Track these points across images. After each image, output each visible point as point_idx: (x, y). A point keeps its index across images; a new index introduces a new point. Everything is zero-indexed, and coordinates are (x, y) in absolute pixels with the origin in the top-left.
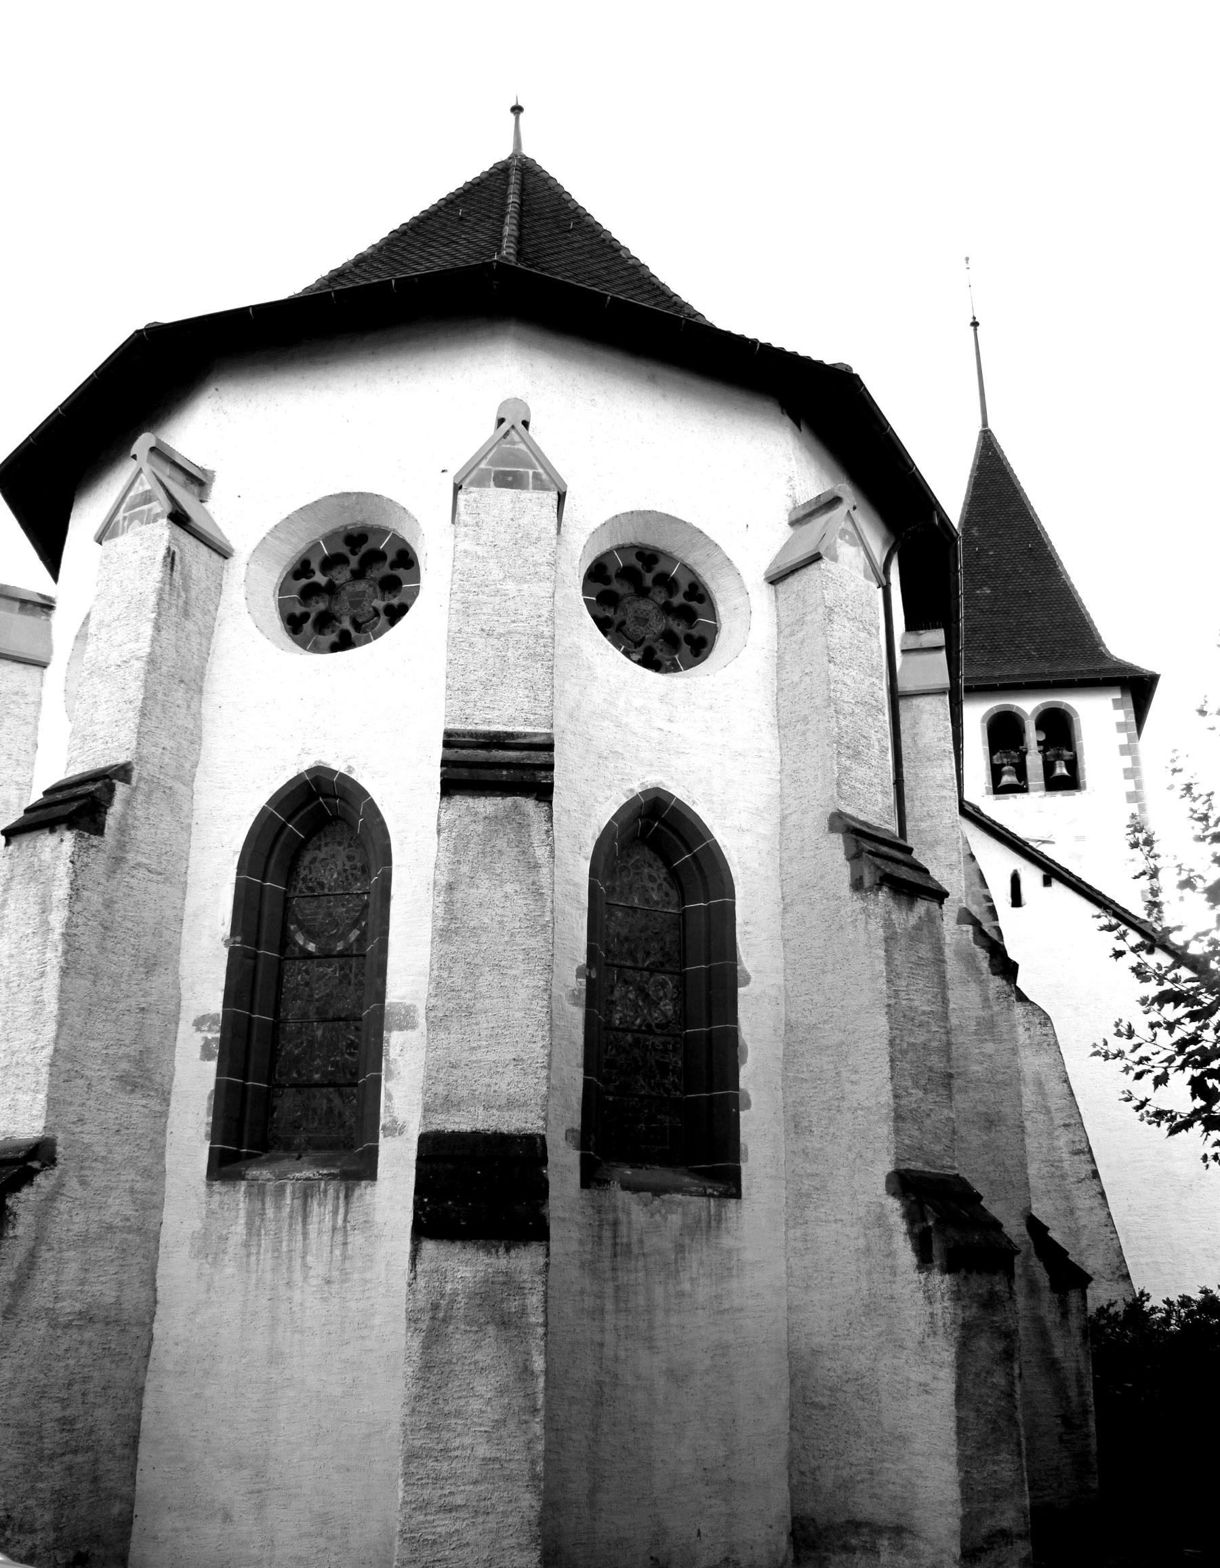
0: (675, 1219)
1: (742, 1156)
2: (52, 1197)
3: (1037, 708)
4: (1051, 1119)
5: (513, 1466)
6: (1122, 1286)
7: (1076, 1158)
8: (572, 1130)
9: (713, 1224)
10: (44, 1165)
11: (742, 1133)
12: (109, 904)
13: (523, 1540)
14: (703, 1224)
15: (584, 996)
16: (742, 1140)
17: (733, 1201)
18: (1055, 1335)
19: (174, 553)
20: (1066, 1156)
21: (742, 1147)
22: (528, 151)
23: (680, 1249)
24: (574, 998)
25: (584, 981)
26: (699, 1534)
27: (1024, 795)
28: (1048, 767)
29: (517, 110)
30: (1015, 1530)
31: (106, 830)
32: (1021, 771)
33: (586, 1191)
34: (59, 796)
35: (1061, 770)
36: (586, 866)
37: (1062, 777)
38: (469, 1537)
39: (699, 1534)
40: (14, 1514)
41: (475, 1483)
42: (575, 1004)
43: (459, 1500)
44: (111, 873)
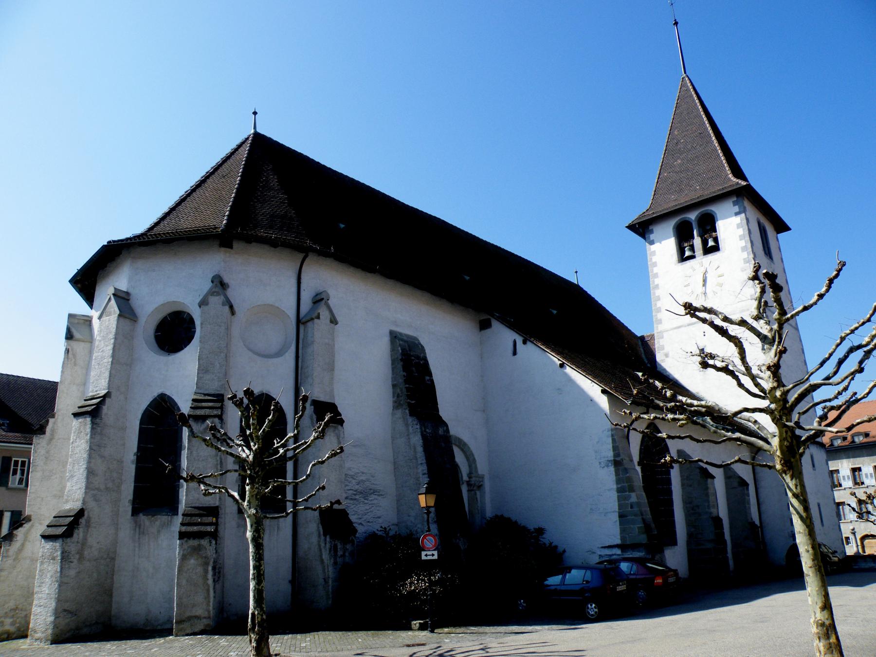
0: (158, 523)
1: (180, 502)
2: (29, 530)
3: (697, 216)
4: (417, 462)
5: (52, 595)
6: (66, 548)
7: (424, 476)
8: (130, 500)
9: (169, 523)
10: (26, 522)
11: (180, 495)
12: (48, 452)
13: (52, 614)
14: (166, 524)
15: (135, 461)
16: (180, 498)
17: (176, 516)
18: (323, 550)
19: (69, 349)
20: (421, 476)
21: (180, 500)
22: (259, 130)
23: (159, 532)
24: (133, 462)
25: (135, 457)
26: (160, 613)
27: (694, 260)
28: (705, 243)
29: (255, 113)
30: (203, 615)
31: (46, 432)
32: (692, 248)
33: (132, 517)
34: (767, 252)
35: (711, 243)
36: (138, 423)
37: (712, 247)
38: (43, 613)
39: (160, 613)
40: (19, 607)
41: (45, 600)
42: (133, 464)
43: (42, 604)
44: (48, 444)
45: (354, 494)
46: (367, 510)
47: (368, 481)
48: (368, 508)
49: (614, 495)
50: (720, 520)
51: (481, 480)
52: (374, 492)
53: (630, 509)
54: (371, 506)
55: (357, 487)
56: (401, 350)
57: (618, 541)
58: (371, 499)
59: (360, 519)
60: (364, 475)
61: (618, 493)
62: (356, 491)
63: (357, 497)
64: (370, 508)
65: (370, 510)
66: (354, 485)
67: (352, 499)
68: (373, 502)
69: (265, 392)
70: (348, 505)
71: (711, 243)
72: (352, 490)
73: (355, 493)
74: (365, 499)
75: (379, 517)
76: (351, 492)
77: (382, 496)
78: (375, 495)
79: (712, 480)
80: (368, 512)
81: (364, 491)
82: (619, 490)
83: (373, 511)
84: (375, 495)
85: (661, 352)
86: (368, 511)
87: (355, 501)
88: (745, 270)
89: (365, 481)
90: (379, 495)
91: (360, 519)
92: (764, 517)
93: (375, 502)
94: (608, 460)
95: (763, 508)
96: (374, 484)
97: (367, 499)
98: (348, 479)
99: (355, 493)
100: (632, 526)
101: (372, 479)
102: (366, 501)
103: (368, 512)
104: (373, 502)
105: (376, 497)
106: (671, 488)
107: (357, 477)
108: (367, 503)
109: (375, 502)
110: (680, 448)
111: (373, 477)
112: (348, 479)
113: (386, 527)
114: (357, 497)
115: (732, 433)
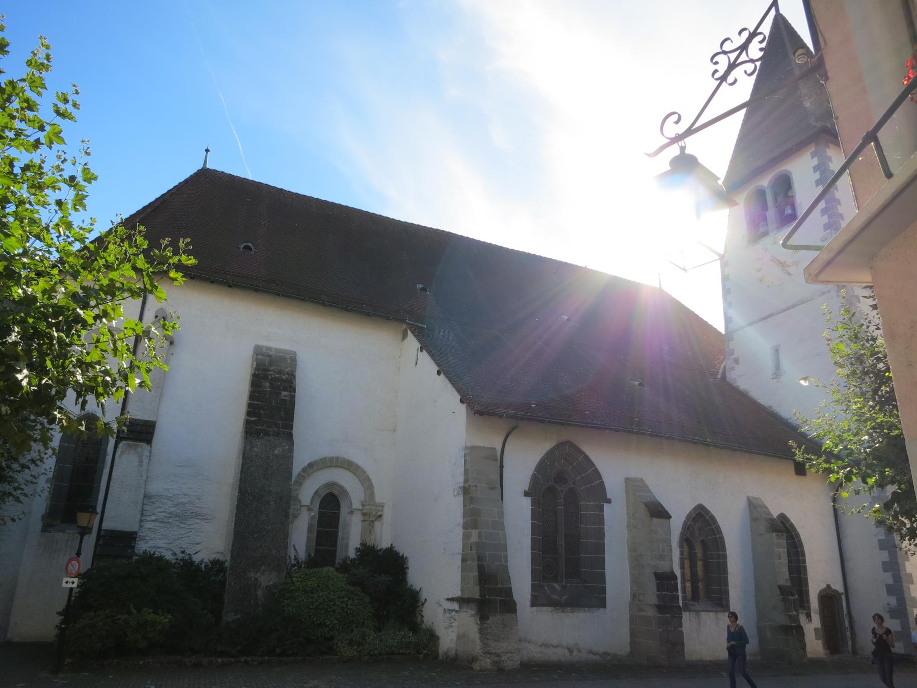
28: (781, 212)
29: (207, 151)
45: (167, 517)
46: (181, 534)
47: (191, 504)
48: (184, 533)
49: (460, 531)
50: (673, 577)
51: (380, 508)
52: (197, 515)
53: (470, 552)
54: (188, 530)
55: (173, 509)
56: (256, 364)
57: (458, 593)
58: (189, 523)
59: (170, 543)
60: (187, 497)
61: (463, 529)
62: (171, 513)
63: (171, 520)
64: (185, 533)
65: (185, 536)
66: (169, 507)
67: (163, 522)
68: (192, 526)
69: (90, 412)
70: (157, 528)
71: (788, 211)
72: (165, 512)
73: (169, 515)
74: (181, 523)
75: (198, 544)
76: (164, 514)
77: (207, 521)
78: (198, 519)
79: (668, 520)
80: (182, 538)
81: (182, 514)
82: (465, 526)
83: (190, 537)
84: (198, 519)
85: (731, 357)
86: (183, 536)
87: (167, 524)
88: (826, 239)
89: (186, 503)
90: (201, 519)
91: (170, 543)
92: (851, 579)
93: (196, 526)
94: (459, 487)
95: (849, 565)
96: (198, 507)
97: (184, 523)
98: (163, 500)
99: (169, 515)
100: (469, 574)
101: (197, 501)
102: (183, 525)
103: (182, 538)
104: (192, 526)
105: (198, 521)
106: (604, 529)
107: (175, 499)
108: (183, 528)
109: (196, 526)
110: (633, 474)
111: (199, 499)
112: (163, 500)
113: (191, 554)
114: (171, 520)
115: (47, 422)
